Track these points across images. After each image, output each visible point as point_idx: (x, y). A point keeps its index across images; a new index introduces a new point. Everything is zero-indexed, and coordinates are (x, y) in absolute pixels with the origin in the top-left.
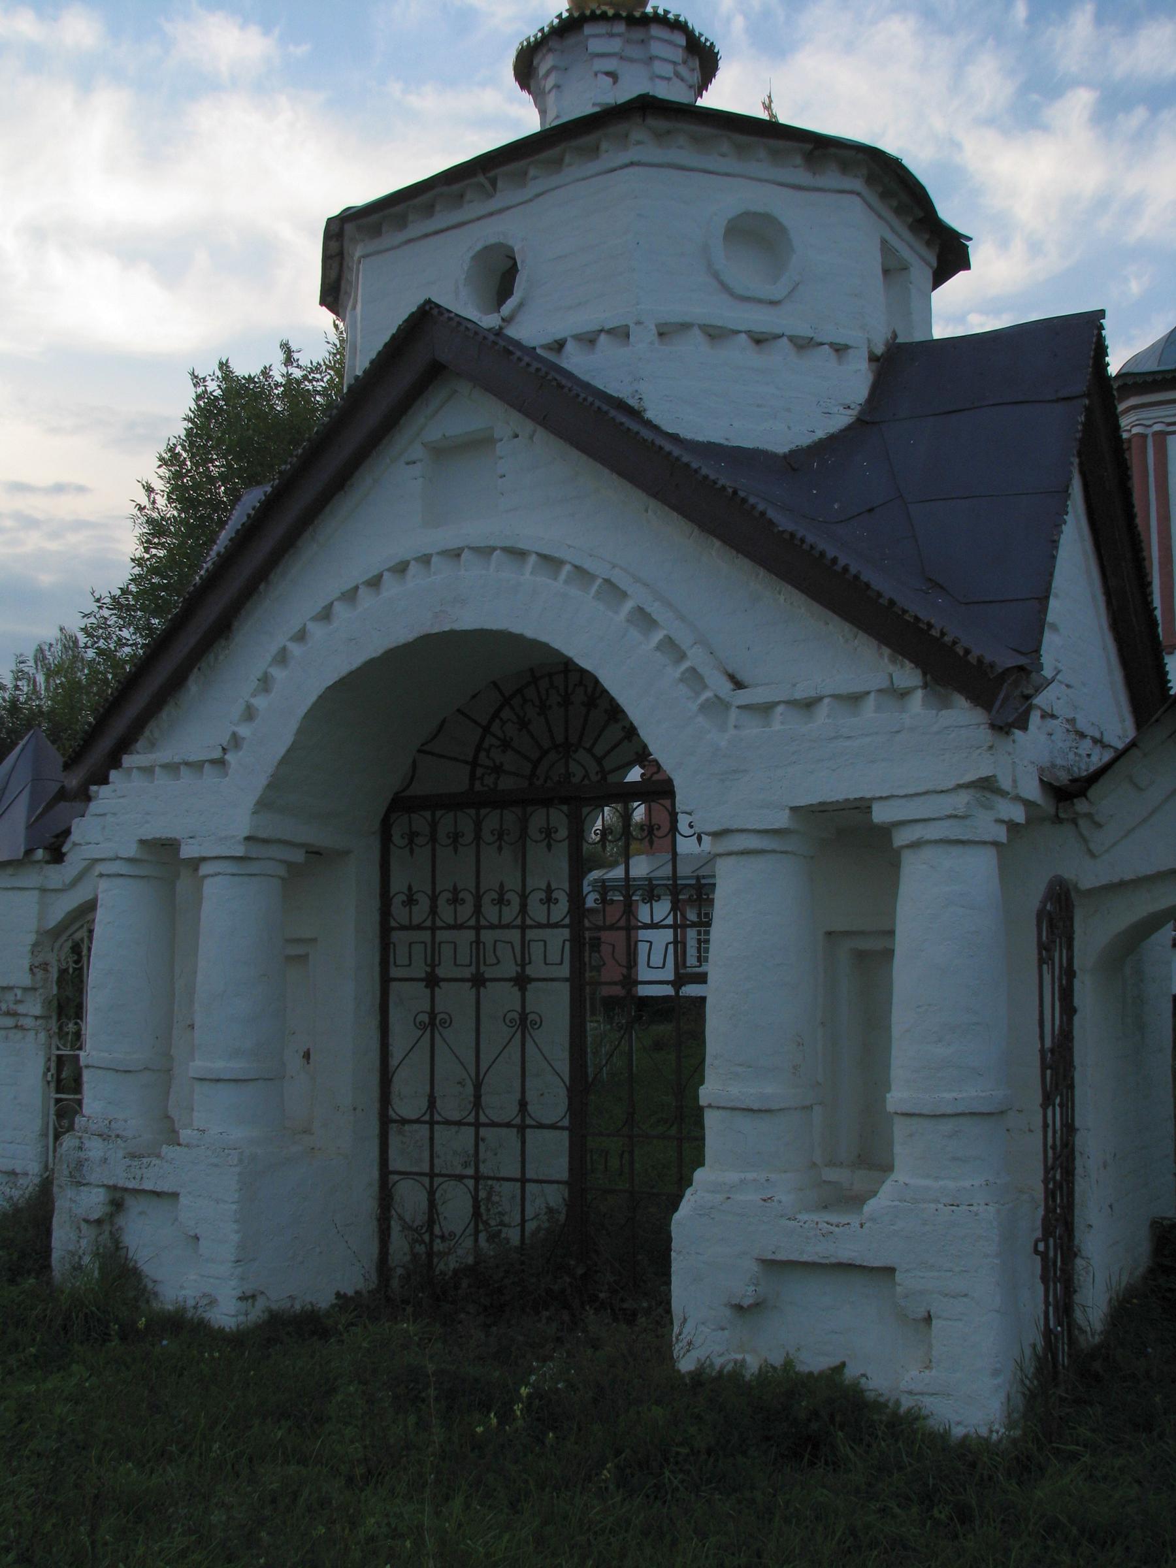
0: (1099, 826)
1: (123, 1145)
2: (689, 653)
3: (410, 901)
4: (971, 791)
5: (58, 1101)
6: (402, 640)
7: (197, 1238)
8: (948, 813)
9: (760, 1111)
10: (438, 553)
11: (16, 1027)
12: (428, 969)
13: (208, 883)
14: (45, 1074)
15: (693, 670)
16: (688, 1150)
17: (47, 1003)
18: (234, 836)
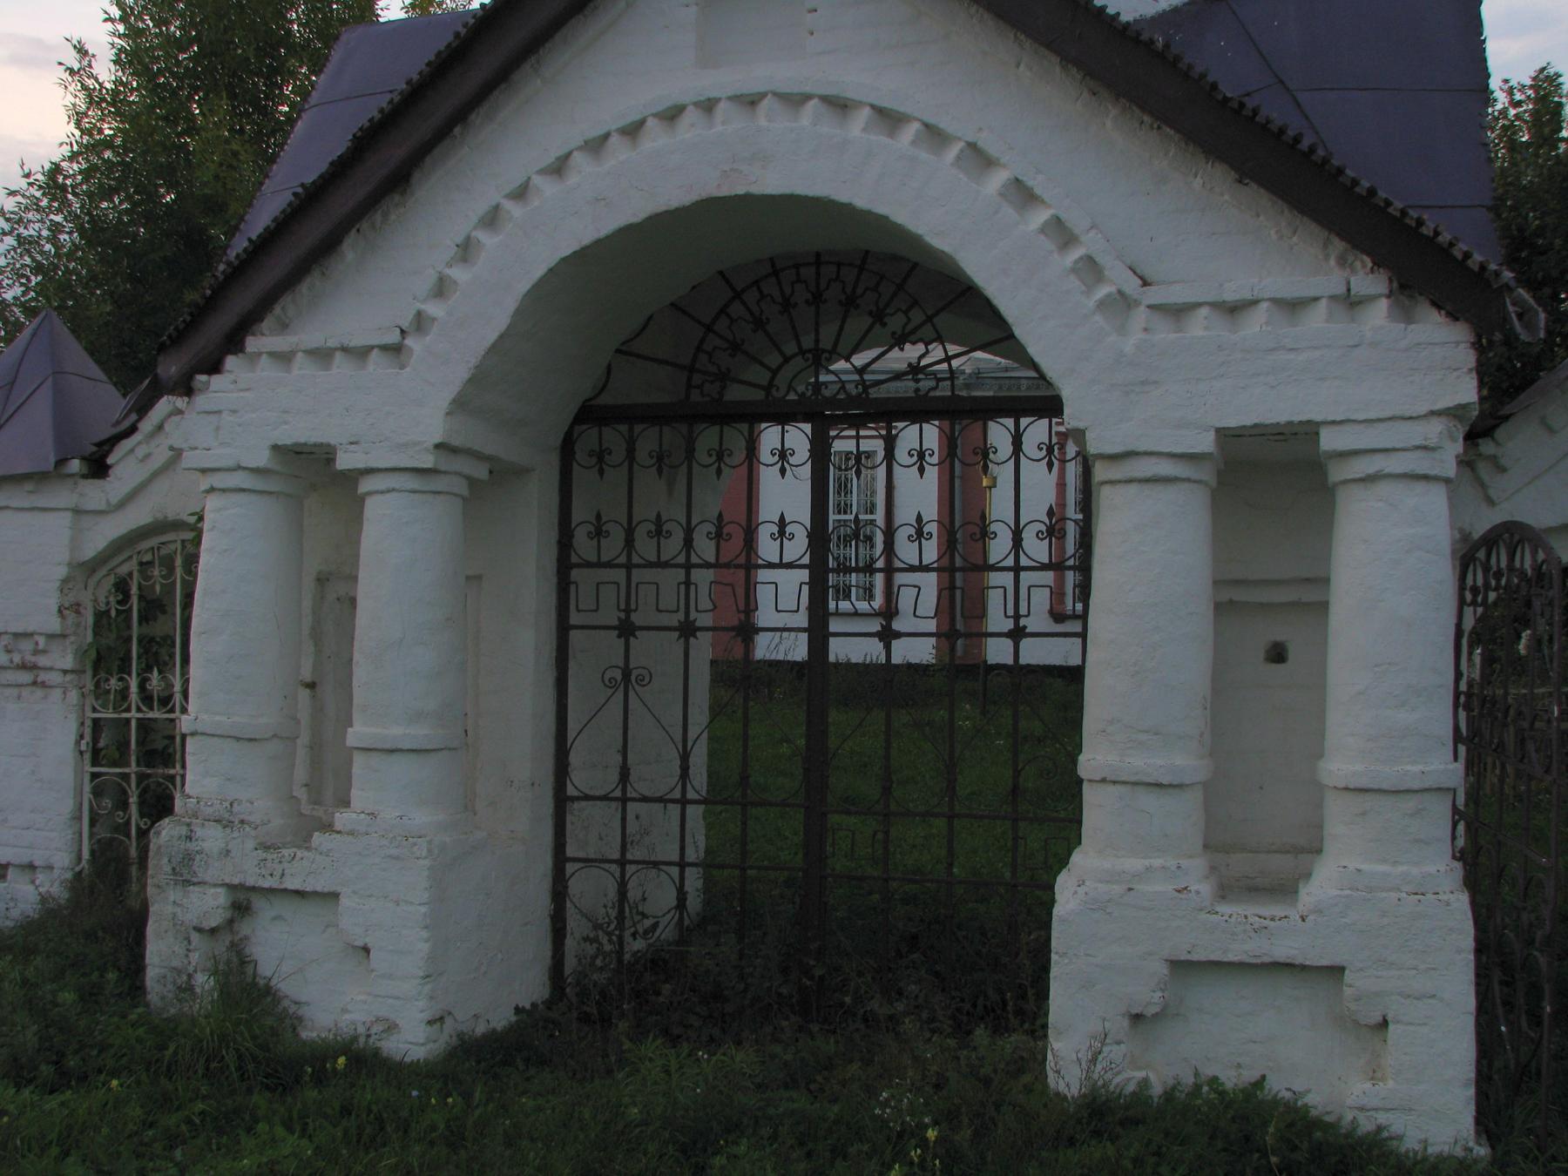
0: (1502, 470)
1: (253, 833)
2: (1083, 238)
3: (599, 533)
4: (1443, 419)
5: (94, 776)
6: (674, 204)
7: (366, 950)
8: (1418, 443)
9: (1170, 786)
10: (730, 98)
11: (35, 683)
12: (623, 615)
13: (370, 503)
14: (78, 743)
15: (1089, 260)
16: (1066, 830)
17: (81, 654)
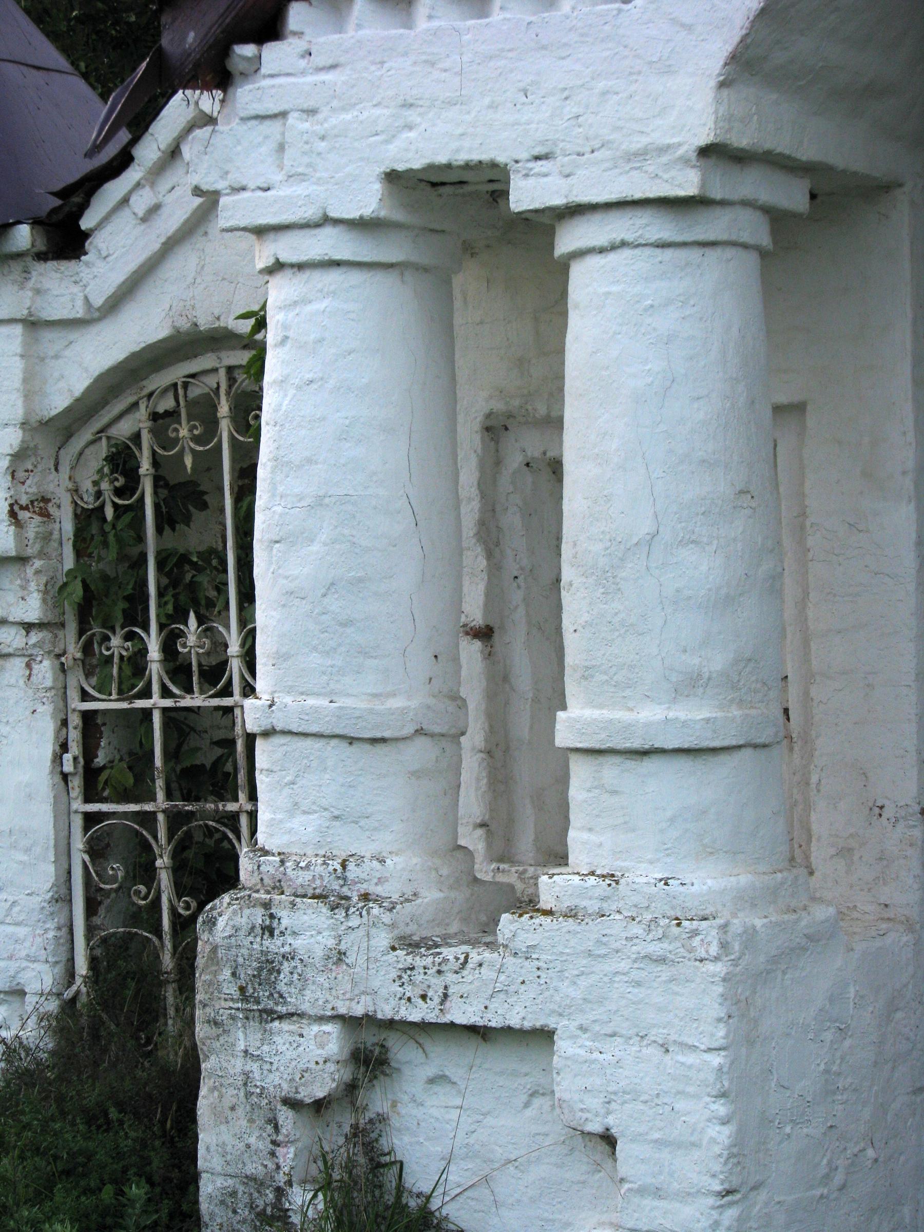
1: (387, 918)
14: (58, 759)
17: (55, 593)
18: (663, 150)
